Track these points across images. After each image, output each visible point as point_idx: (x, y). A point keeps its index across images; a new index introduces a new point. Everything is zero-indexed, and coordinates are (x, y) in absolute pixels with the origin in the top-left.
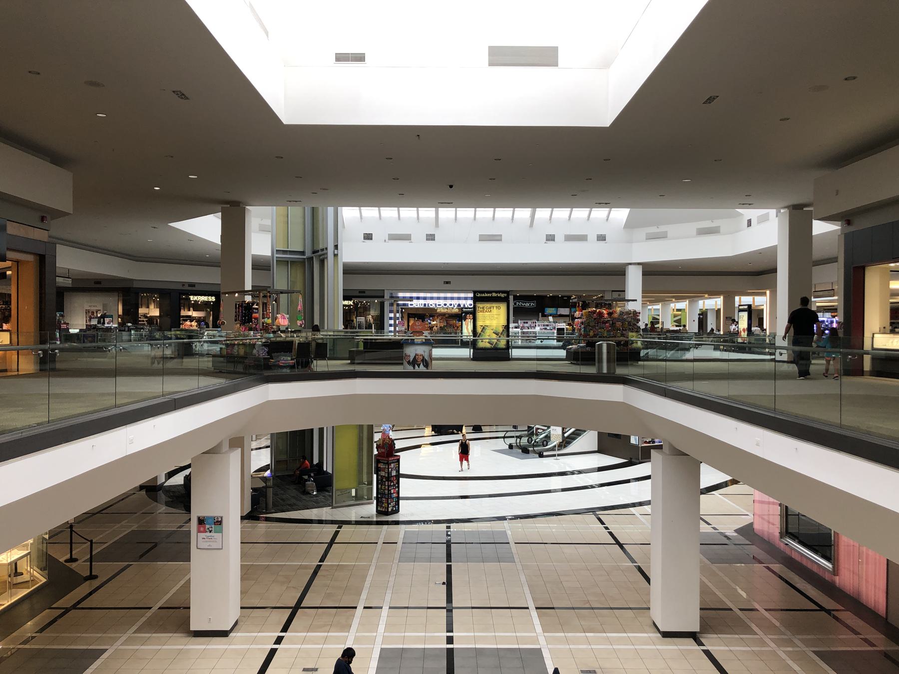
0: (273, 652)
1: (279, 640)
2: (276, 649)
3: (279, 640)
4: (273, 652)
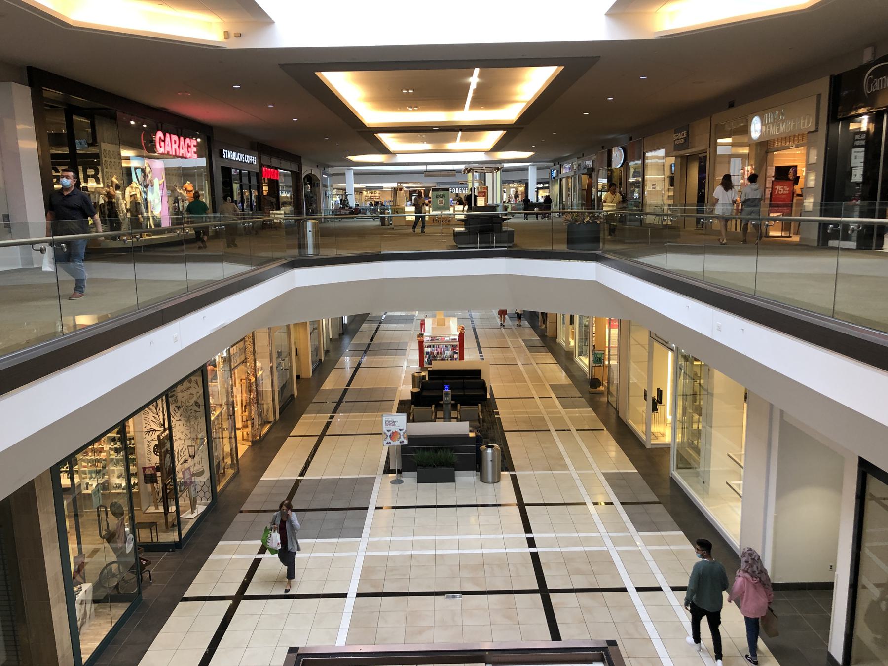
2: (331, 422)
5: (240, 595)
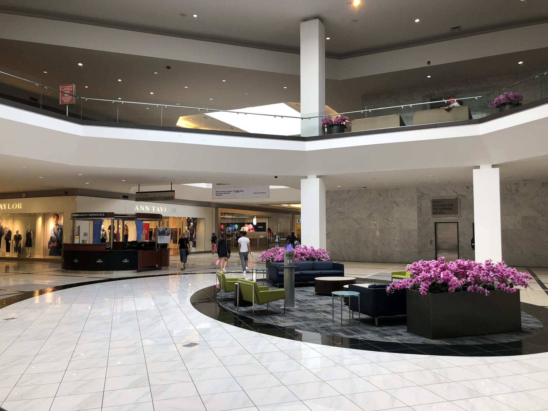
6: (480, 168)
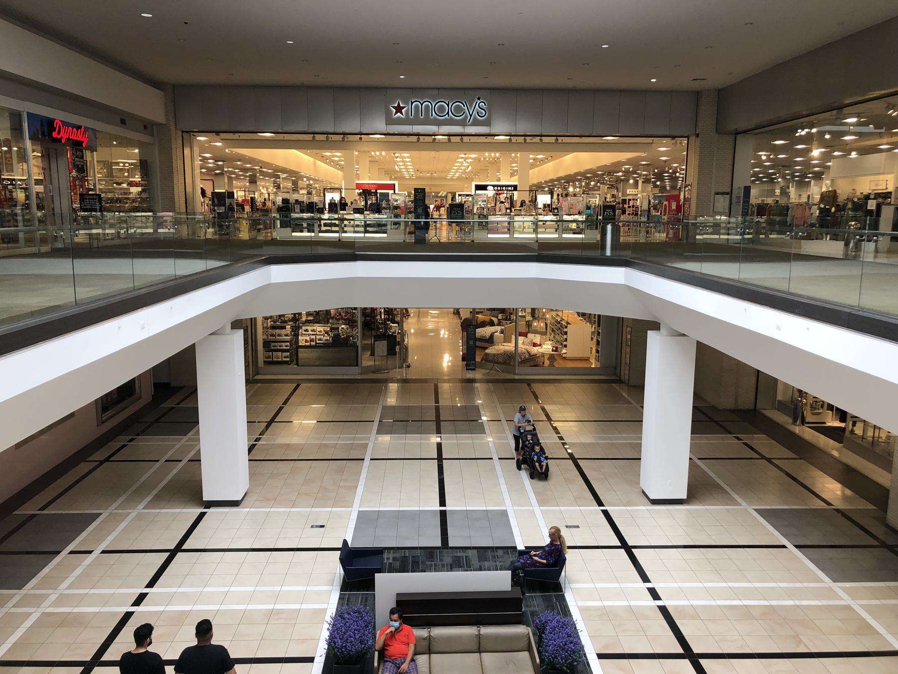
0: (151, 584)
1: (140, 599)
2: (205, 513)
3: (140, 599)
4: (151, 584)
5: (179, 548)
6: (397, 594)
